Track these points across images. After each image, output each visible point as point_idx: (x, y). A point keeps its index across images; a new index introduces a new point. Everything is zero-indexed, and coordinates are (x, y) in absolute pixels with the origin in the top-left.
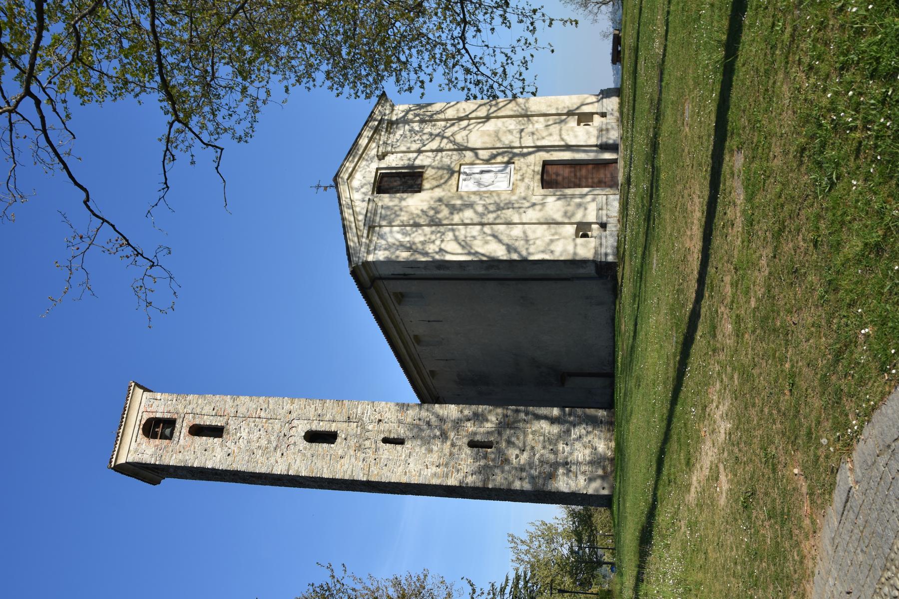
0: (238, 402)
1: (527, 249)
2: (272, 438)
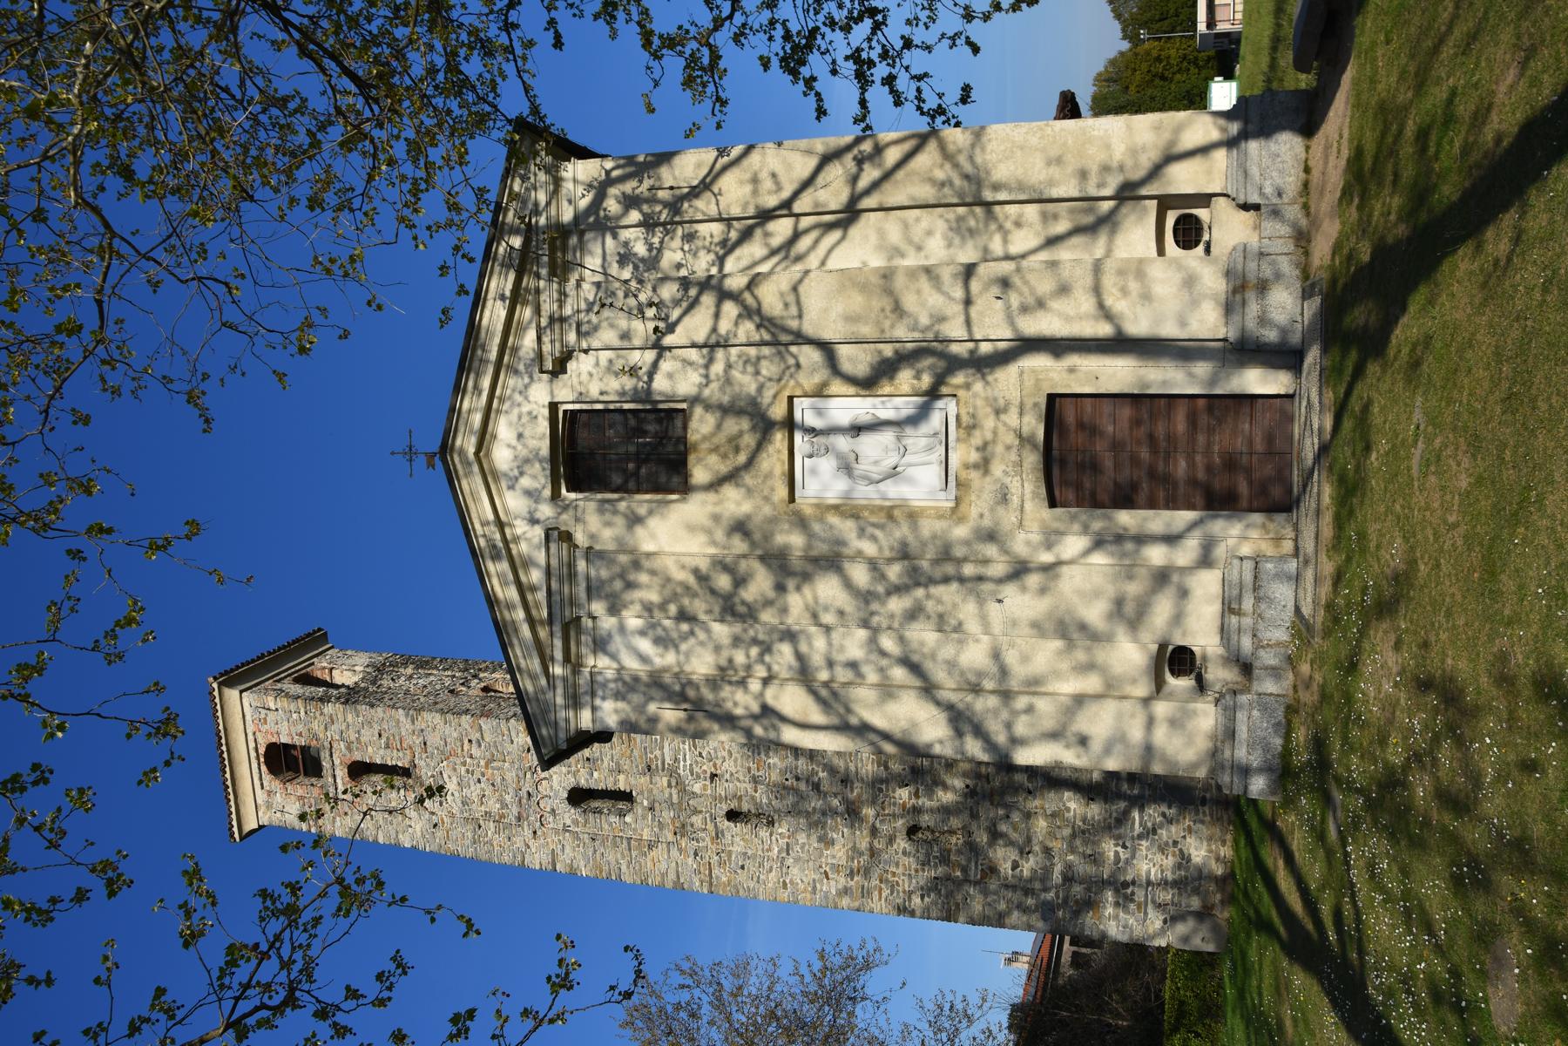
0: (420, 724)
1: (1009, 726)
2: (508, 798)
